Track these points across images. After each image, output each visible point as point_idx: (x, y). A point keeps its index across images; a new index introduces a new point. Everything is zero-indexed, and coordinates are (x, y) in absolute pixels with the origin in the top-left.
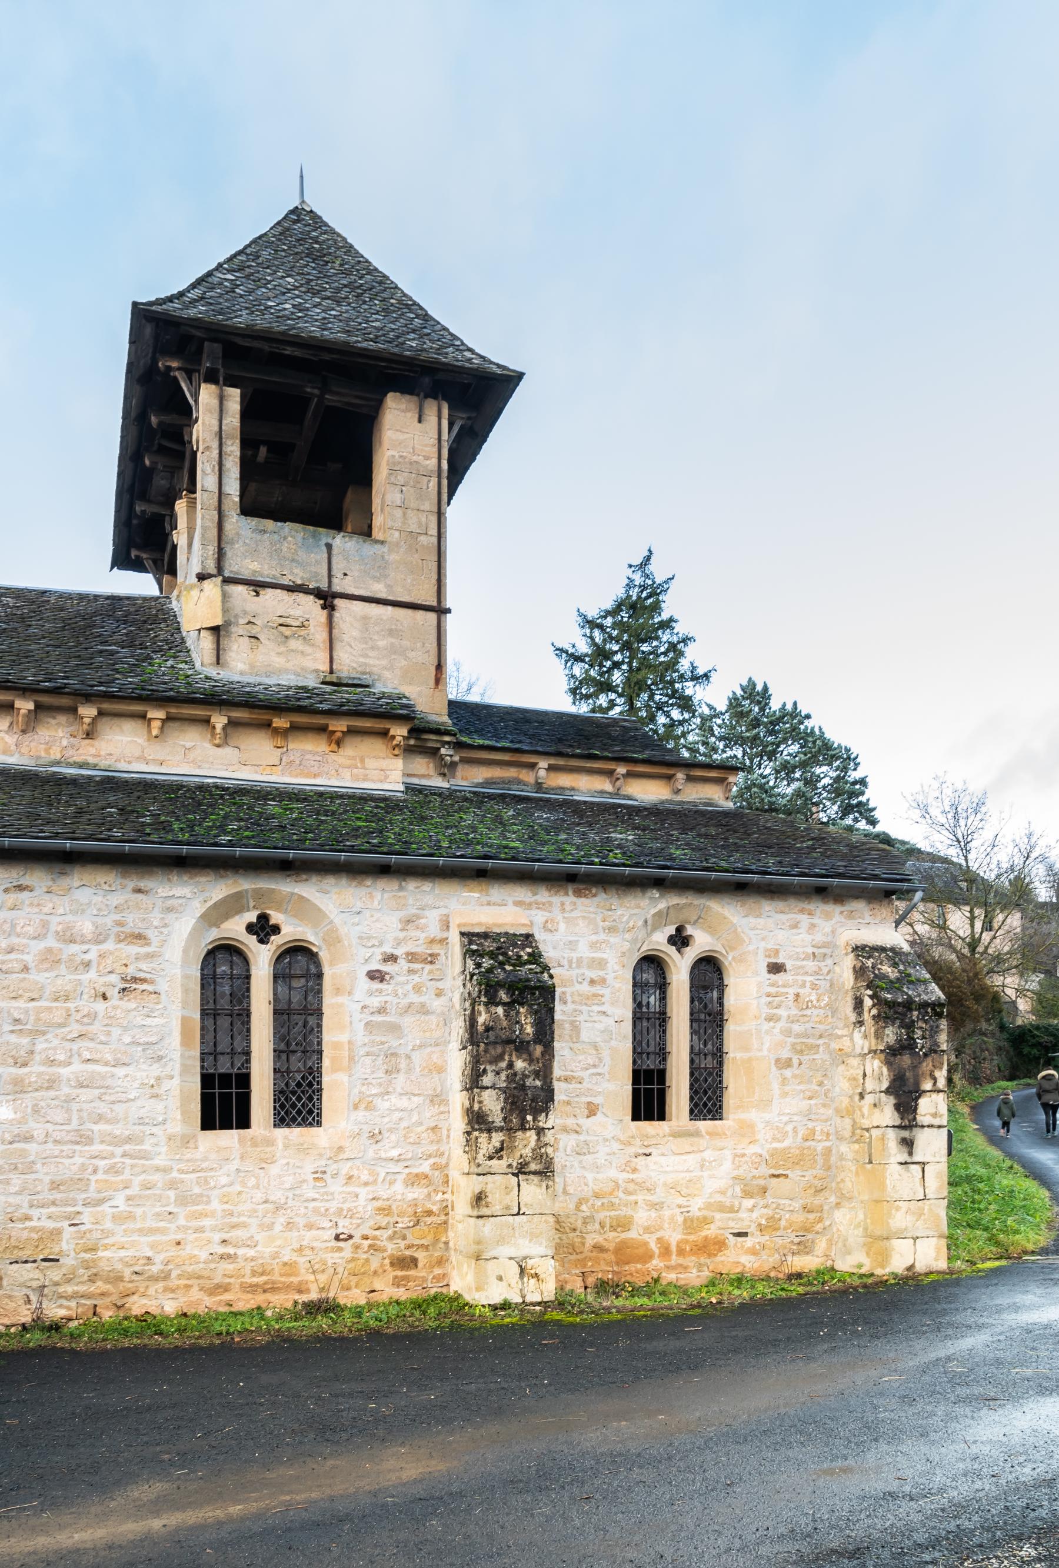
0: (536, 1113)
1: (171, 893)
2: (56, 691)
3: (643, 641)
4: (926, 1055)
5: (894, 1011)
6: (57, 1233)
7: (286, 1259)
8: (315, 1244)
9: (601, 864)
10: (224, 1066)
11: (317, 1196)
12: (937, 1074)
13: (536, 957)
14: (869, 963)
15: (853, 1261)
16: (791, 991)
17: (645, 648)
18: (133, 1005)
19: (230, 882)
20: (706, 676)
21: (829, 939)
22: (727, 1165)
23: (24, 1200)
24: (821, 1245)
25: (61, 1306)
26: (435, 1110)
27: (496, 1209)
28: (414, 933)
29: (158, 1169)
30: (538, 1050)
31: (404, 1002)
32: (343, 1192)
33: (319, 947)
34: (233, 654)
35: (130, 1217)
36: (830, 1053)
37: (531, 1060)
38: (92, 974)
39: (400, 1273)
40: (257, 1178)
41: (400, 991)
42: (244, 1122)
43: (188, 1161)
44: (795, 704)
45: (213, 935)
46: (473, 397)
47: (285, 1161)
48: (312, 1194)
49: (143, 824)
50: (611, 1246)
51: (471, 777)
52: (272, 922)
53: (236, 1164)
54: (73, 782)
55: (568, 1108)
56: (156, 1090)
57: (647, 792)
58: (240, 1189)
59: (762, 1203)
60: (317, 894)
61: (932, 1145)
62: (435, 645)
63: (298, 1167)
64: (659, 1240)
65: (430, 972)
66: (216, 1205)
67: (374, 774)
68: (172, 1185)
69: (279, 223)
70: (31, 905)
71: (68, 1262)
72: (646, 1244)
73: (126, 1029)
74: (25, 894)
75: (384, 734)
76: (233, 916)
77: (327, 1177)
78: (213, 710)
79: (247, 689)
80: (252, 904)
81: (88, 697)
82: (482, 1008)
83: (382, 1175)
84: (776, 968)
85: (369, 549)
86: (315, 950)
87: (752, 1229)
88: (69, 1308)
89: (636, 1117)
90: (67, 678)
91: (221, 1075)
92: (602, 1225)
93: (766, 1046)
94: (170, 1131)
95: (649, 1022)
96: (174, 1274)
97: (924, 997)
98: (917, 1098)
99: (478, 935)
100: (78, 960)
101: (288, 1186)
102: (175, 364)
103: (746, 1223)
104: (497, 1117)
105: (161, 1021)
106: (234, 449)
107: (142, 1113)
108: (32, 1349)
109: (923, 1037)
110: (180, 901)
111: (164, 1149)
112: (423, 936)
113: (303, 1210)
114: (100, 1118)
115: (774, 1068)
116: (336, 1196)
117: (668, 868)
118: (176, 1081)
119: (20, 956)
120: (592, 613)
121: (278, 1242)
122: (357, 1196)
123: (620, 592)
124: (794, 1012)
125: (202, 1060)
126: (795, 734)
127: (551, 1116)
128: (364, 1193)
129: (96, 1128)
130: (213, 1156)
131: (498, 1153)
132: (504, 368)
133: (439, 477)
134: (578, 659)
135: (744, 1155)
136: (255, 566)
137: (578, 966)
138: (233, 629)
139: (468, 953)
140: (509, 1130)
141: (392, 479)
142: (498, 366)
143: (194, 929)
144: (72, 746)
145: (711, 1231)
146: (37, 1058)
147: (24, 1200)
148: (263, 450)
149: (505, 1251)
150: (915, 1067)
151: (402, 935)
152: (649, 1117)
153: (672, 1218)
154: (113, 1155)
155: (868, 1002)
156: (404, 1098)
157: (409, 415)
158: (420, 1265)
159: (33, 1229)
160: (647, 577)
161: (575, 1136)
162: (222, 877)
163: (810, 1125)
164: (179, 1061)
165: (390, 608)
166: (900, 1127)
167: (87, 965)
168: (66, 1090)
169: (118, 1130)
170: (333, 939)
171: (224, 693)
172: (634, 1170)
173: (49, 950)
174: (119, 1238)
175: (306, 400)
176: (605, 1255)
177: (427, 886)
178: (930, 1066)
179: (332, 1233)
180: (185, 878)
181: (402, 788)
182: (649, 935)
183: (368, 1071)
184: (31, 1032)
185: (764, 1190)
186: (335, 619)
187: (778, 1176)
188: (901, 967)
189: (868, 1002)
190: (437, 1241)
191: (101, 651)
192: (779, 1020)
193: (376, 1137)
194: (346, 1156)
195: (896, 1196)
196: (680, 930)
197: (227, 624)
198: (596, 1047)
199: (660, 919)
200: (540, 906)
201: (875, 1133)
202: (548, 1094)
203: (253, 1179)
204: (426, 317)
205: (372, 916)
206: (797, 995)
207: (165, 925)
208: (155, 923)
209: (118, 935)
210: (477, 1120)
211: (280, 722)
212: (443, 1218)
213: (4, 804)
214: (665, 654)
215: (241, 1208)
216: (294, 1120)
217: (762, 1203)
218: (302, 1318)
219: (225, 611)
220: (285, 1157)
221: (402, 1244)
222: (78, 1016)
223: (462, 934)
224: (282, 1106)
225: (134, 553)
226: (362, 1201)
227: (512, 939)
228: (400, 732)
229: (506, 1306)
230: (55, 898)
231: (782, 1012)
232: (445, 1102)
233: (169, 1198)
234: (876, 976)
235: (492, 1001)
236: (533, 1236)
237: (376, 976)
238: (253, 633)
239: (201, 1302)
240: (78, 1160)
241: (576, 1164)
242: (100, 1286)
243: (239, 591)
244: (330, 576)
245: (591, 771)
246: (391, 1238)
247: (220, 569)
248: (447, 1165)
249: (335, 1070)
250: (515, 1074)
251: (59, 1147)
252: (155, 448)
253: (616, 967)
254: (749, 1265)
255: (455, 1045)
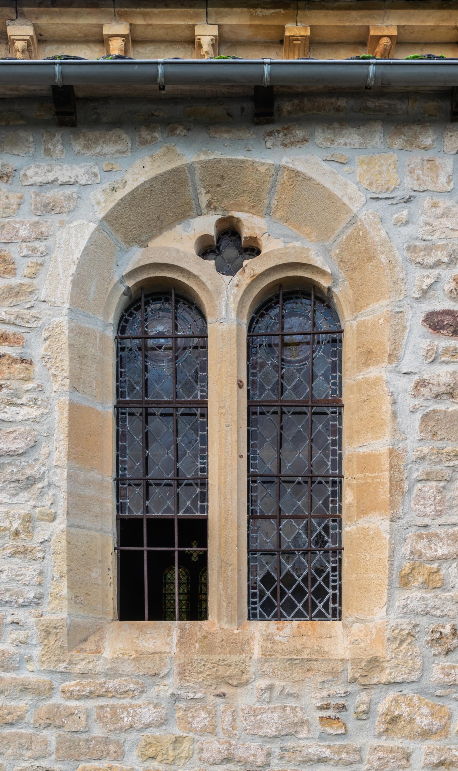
1: (50, 177)
10: (161, 507)
11: (328, 753)
19: (160, 152)
29: (25, 689)
32: (379, 748)
33: (334, 278)
40: (212, 713)
42: (196, 609)
43: (82, 675)
47: (263, 683)
48: (316, 749)
58: (178, 732)
60: (326, 166)
63: (289, 695)
68: (52, 720)
76: (171, 225)
77: (349, 717)
78: (197, 16)
80: (204, 199)
86: (324, 283)
91: (152, 522)
94: (47, 617)
101: (270, 731)
105: (33, 412)
110: (68, 191)
116: (367, 756)
118: (60, 525)
122: (407, 757)
130: (128, 668)
162: (144, 143)
164: (64, 485)
170: (360, 254)
183: (430, 510)
203: (203, 715)
205: (435, 205)
207: (41, 237)
208: (23, 233)
213: (454, 667)
216: (289, 607)
220: (264, 675)
233: (46, 743)
249: (363, 511)
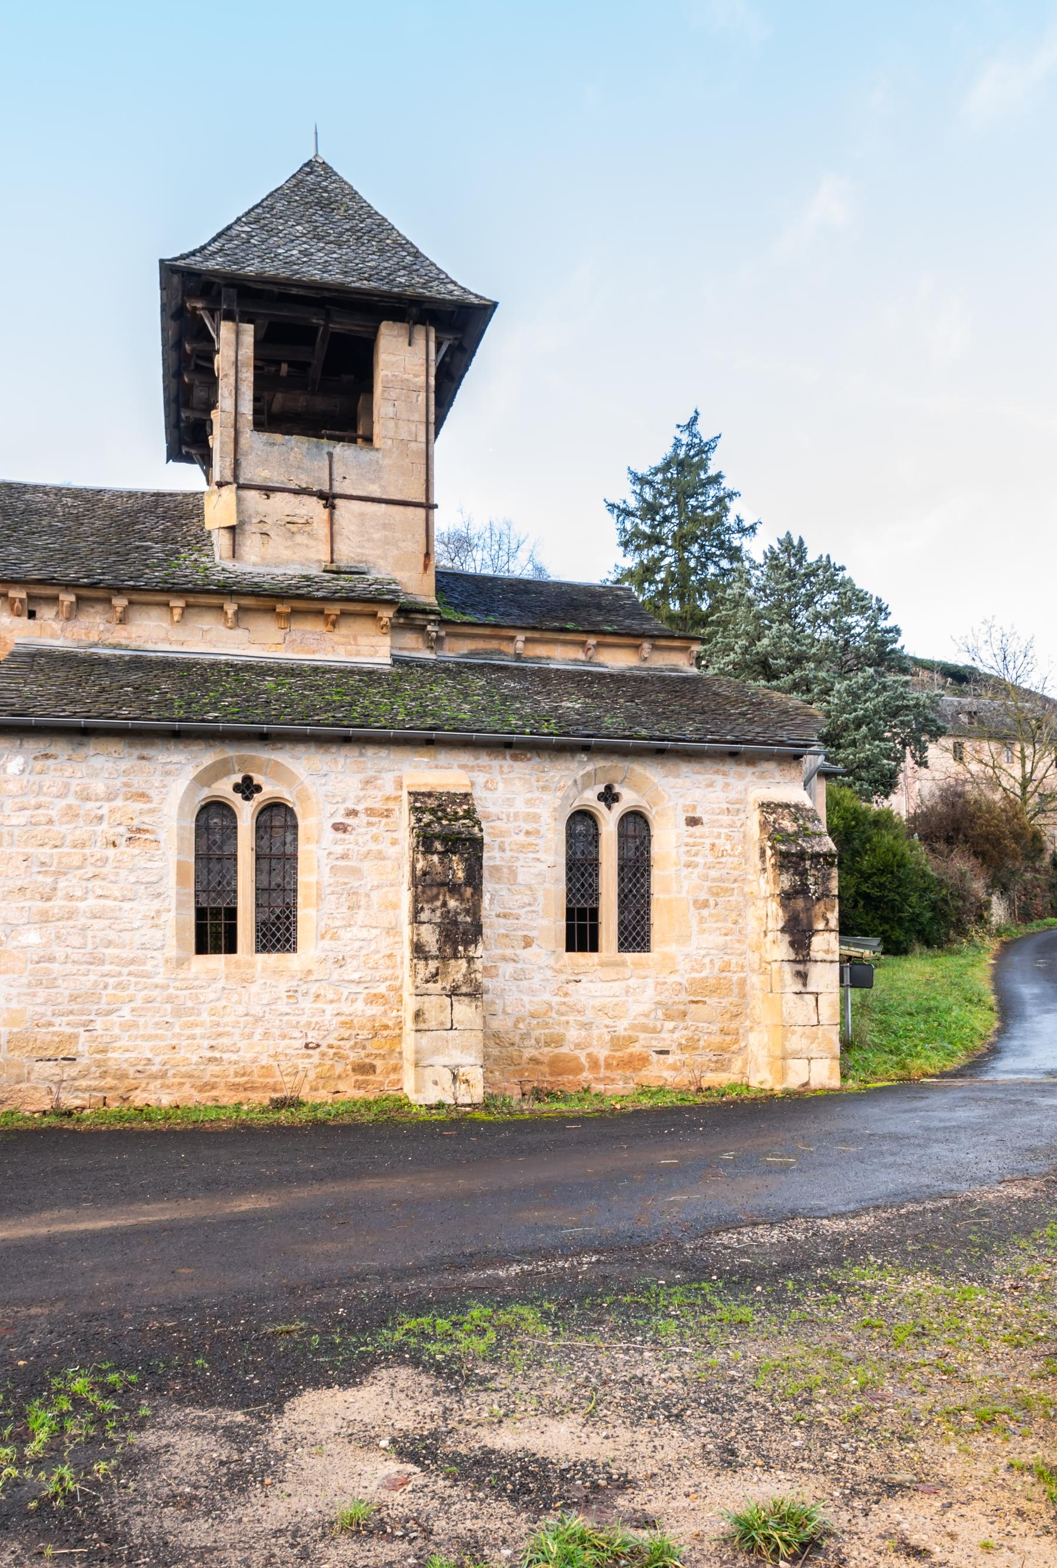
0: (467, 944)
2: (92, 586)
3: (692, 497)
4: (818, 899)
5: (790, 861)
6: (74, 1037)
7: (264, 1063)
8: (288, 1051)
9: (532, 733)
12: (829, 915)
13: (469, 814)
14: (771, 818)
15: (762, 1077)
16: (708, 842)
17: (693, 502)
18: (137, 851)
20: (753, 528)
21: (742, 796)
22: (650, 992)
23: (48, 1010)
24: (737, 1064)
25: (76, 1097)
26: (391, 940)
27: (433, 1024)
28: (375, 792)
29: (156, 986)
30: (469, 891)
31: (364, 850)
34: (246, 549)
35: (135, 1025)
36: (744, 895)
37: (462, 900)
38: (104, 826)
39: (361, 1078)
40: (240, 995)
41: (360, 841)
44: (828, 557)
45: (205, 794)
46: (457, 326)
49: (150, 702)
50: (546, 1060)
51: (456, 650)
52: (255, 782)
53: (221, 983)
54: (106, 662)
55: (507, 941)
56: (156, 921)
57: (617, 660)
59: (682, 1025)
61: (826, 978)
62: (424, 536)
64: (589, 1055)
65: (386, 824)
66: (205, 1017)
67: (365, 650)
69: (294, 176)
70: (55, 770)
71: (83, 1061)
72: (577, 1058)
73: (132, 871)
74: (51, 761)
75: (374, 615)
79: (256, 580)
80: (237, 768)
81: (120, 591)
82: (420, 856)
83: (346, 994)
84: (693, 822)
85: (371, 455)
87: (674, 1048)
88: (83, 1099)
89: (570, 948)
90: (103, 574)
92: (538, 1041)
93: (685, 888)
94: (167, 955)
95: (581, 869)
96: (170, 1073)
97: (817, 849)
98: (810, 937)
99: (423, 794)
100: (93, 814)
102: (199, 305)
103: (668, 1042)
104: (433, 948)
106: (248, 375)
107: (144, 939)
108: (44, 1129)
109: (816, 884)
111: (162, 970)
112: (380, 794)
113: (277, 1023)
114: (109, 944)
115: (692, 908)
117: (592, 736)
118: (173, 913)
119: (45, 812)
120: (643, 470)
121: (257, 1049)
123: (668, 451)
124: (711, 859)
125: (197, 896)
126: (830, 584)
127: (480, 947)
128: (330, 1009)
129: (107, 951)
131: (434, 977)
132: (482, 298)
133: (427, 391)
134: (629, 514)
135: (665, 983)
136: (266, 473)
137: (515, 820)
138: (247, 527)
139: (414, 810)
140: (443, 958)
141: (386, 395)
142: (477, 296)
143: (188, 788)
144: (108, 630)
145: (636, 1049)
146: (60, 894)
147: (48, 1010)
148: (284, 367)
149: (440, 1060)
150: (808, 910)
151: (362, 793)
152: (582, 949)
153: (600, 1037)
154: (120, 974)
155: (769, 852)
156: (365, 930)
157: (401, 339)
158: (378, 1071)
159: (54, 1034)
160: (695, 436)
161: (512, 964)
163: (726, 958)
165: (384, 505)
166: (794, 961)
167: (101, 818)
168: (82, 921)
169: (125, 953)
171: (234, 584)
172: (566, 994)
173: (70, 807)
174: (124, 1043)
175: (316, 329)
176: (540, 1067)
177: (383, 753)
178: (823, 909)
179: (303, 1042)
180: (181, 747)
181: (390, 661)
182: (581, 792)
184: (54, 872)
185: (684, 1014)
186: (336, 517)
187: (697, 1002)
188: (801, 822)
189: (769, 852)
190: (392, 1051)
191: (138, 547)
192: (696, 866)
193: (341, 963)
194: (314, 978)
195: (792, 1022)
196: (609, 788)
197: (242, 523)
198: (530, 888)
199: (588, 780)
200: (480, 769)
201: (775, 966)
202: (477, 930)
204: (417, 254)
206: (713, 845)
207: (164, 786)
209: (125, 794)
210: (419, 950)
211: (281, 608)
212: (398, 1031)
214: (712, 508)
215: (225, 1020)
216: (274, 947)
217: (682, 1025)
218: (268, 1111)
219: (240, 512)
221: (363, 1053)
222: (93, 860)
223: (410, 793)
224: (264, 935)
225: (184, 450)
226: (328, 1016)
227: (452, 798)
228: (386, 614)
229: (440, 1106)
230: (75, 764)
231: (700, 860)
232: (399, 934)
234: (775, 829)
235: (429, 850)
236: (464, 1048)
237: (338, 827)
238: (264, 530)
239: (189, 1096)
240: (92, 978)
241: (514, 988)
242: (110, 1081)
243: (252, 496)
244: (331, 480)
245: (565, 643)
246: (353, 1048)
247: (236, 477)
248: (401, 987)
250: (448, 912)
251: (77, 967)
252: (192, 367)
253: (549, 821)
254: (670, 1080)
255: (406, 886)
